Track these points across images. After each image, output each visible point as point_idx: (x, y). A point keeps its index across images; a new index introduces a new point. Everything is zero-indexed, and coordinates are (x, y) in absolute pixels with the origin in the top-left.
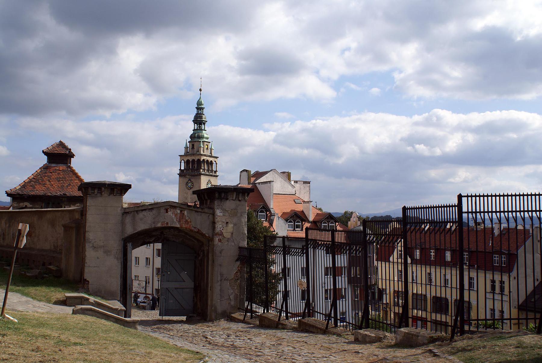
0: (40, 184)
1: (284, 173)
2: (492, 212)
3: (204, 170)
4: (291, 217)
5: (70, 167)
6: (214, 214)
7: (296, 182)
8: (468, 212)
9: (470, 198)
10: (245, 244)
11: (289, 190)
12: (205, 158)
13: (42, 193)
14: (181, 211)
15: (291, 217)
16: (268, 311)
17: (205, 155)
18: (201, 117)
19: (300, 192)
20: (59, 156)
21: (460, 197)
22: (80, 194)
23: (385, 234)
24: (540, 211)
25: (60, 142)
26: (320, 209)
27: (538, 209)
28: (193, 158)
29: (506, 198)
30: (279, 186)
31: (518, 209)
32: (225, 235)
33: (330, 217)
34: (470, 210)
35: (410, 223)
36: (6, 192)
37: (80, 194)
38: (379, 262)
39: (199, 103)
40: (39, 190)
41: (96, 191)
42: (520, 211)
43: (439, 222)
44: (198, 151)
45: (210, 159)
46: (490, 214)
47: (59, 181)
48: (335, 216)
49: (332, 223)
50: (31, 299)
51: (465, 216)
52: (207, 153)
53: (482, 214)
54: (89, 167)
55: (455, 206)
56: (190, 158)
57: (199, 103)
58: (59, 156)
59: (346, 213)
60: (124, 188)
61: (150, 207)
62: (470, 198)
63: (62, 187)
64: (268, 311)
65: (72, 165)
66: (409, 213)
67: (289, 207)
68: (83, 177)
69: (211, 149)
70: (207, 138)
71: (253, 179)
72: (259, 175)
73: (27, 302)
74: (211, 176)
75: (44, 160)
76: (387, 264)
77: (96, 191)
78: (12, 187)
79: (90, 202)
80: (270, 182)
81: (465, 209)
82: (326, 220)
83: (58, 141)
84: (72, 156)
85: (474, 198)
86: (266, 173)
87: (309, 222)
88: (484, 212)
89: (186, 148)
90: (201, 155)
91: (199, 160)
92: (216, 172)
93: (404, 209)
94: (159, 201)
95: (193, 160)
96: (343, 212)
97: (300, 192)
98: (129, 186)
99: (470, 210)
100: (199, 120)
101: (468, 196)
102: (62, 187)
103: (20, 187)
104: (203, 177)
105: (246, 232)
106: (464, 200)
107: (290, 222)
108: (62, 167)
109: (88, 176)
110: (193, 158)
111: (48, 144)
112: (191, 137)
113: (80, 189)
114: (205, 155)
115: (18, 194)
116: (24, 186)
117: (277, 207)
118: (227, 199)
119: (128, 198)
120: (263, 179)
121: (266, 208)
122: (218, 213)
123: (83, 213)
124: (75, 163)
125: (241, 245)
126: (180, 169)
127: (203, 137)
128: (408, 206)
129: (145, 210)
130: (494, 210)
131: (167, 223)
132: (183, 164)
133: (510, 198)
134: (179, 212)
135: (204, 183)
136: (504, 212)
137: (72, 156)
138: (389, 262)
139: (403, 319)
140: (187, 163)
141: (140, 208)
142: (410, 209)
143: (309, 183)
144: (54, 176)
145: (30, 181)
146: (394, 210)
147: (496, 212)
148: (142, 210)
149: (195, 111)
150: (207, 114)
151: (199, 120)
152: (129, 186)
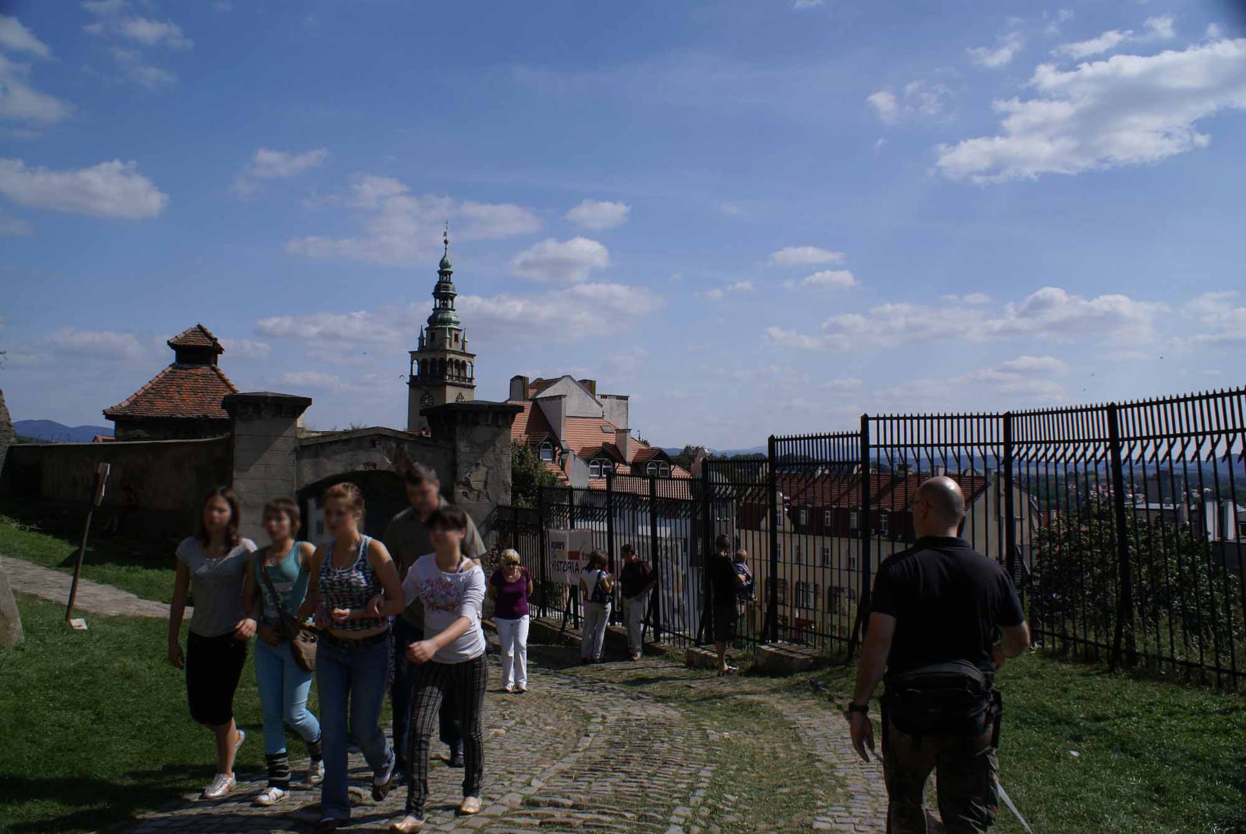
0: (163, 397)
1: (584, 381)
2: (946, 445)
3: (451, 376)
4: (596, 456)
5: (214, 369)
6: (454, 450)
7: (604, 397)
8: (878, 446)
9: (881, 422)
10: (507, 499)
11: (595, 410)
12: (452, 356)
13: (166, 414)
14: (398, 445)
15: (596, 456)
16: (544, 615)
17: (453, 352)
18: (447, 288)
19: (611, 414)
20: (197, 352)
21: (865, 420)
22: (224, 415)
23: (753, 484)
24: (1242, 430)
25: (199, 326)
26: (645, 443)
27: (1238, 426)
28: (432, 356)
29: (942, 421)
30: (576, 403)
31: (962, 441)
32: (473, 484)
33: (660, 455)
34: (882, 443)
35: (1018, 443)
36: (104, 412)
37: (224, 415)
38: (743, 531)
39: (444, 264)
40: (162, 409)
41: (250, 410)
42: (966, 445)
43: (848, 462)
44: (443, 345)
45: (462, 359)
46: (969, 448)
47: (196, 393)
48: (669, 454)
49: (664, 465)
50: (135, 596)
51: (873, 453)
52: (457, 347)
53: (902, 449)
54: (246, 369)
55: (857, 435)
56: (428, 357)
57: (444, 264)
58: (197, 352)
59: (687, 448)
60: (301, 404)
61: (345, 437)
62: (881, 422)
63: (202, 404)
64: (544, 615)
65: (219, 366)
66: (780, 451)
67: (596, 440)
68: (236, 388)
69: (464, 342)
70: (457, 323)
71: (531, 392)
72: (542, 384)
73: (127, 600)
74: (464, 386)
75: (172, 354)
76: (757, 533)
77: (250, 410)
78: (115, 404)
79: (239, 428)
80: (560, 397)
81: (873, 441)
82: (655, 462)
83: (194, 326)
84: (220, 350)
85: (888, 422)
86: (555, 381)
87: (625, 463)
88: (906, 446)
89: (421, 339)
90: (448, 351)
91: (443, 360)
92: (471, 380)
93: (772, 440)
94: (361, 427)
95: (434, 360)
96: (683, 448)
97: (611, 414)
98: (307, 402)
99: (882, 443)
100: (443, 293)
101: (878, 419)
102: (202, 404)
103: (127, 403)
104: (448, 389)
105: (510, 480)
106: (872, 424)
107: (594, 463)
108: (204, 369)
109: (245, 384)
110: (432, 356)
111: (179, 327)
112: (431, 320)
113: (225, 404)
114: (453, 352)
115: (125, 415)
116: (135, 401)
117: (574, 437)
118: (477, 424)
119: (310, 422)
120: (548, 392)
121: (555, 441)
122: (463, 447)
123: (229, 445)
124: (222, 362)
125: (500, 503)
126: (411, 375)
127: (449, 321)
128: (777, 435)
129: (336, 442)
130: (936, 442)
131: (375, 465)
132: (416, 367)
133: (949, 421)
134: (394, 445)
135: (451, 395)
136: (952, 445)
137: (220, 350)
138: (759, 529)
139: (771, 630)
140: (422, 365)
141: (328, 440)
142: (781, 440)
143: (626, 398)
144: (189, 384)
145: (146, 392)
146: (758, 445)
147: (925, 445)
148: (331, 443)
149: (436, 278)
150: (456, 282)
151: (443, 293)
152: (307, 402)
